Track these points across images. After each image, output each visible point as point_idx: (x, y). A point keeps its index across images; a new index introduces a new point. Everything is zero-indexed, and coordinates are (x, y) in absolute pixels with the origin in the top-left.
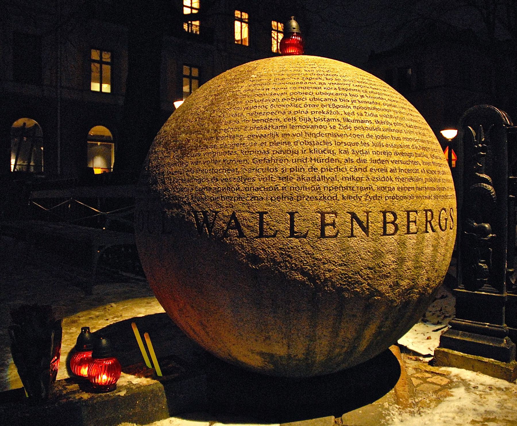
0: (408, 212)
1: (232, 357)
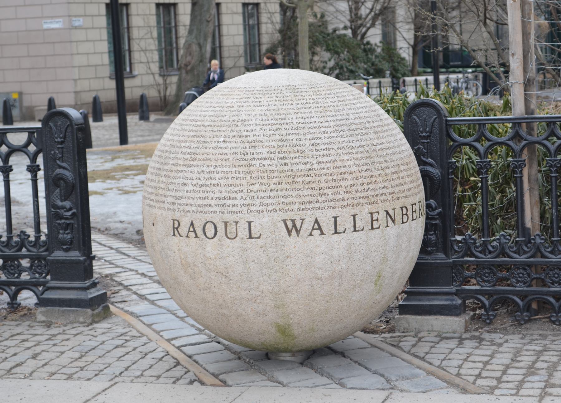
0: (372, 214)
1: (259, 350)
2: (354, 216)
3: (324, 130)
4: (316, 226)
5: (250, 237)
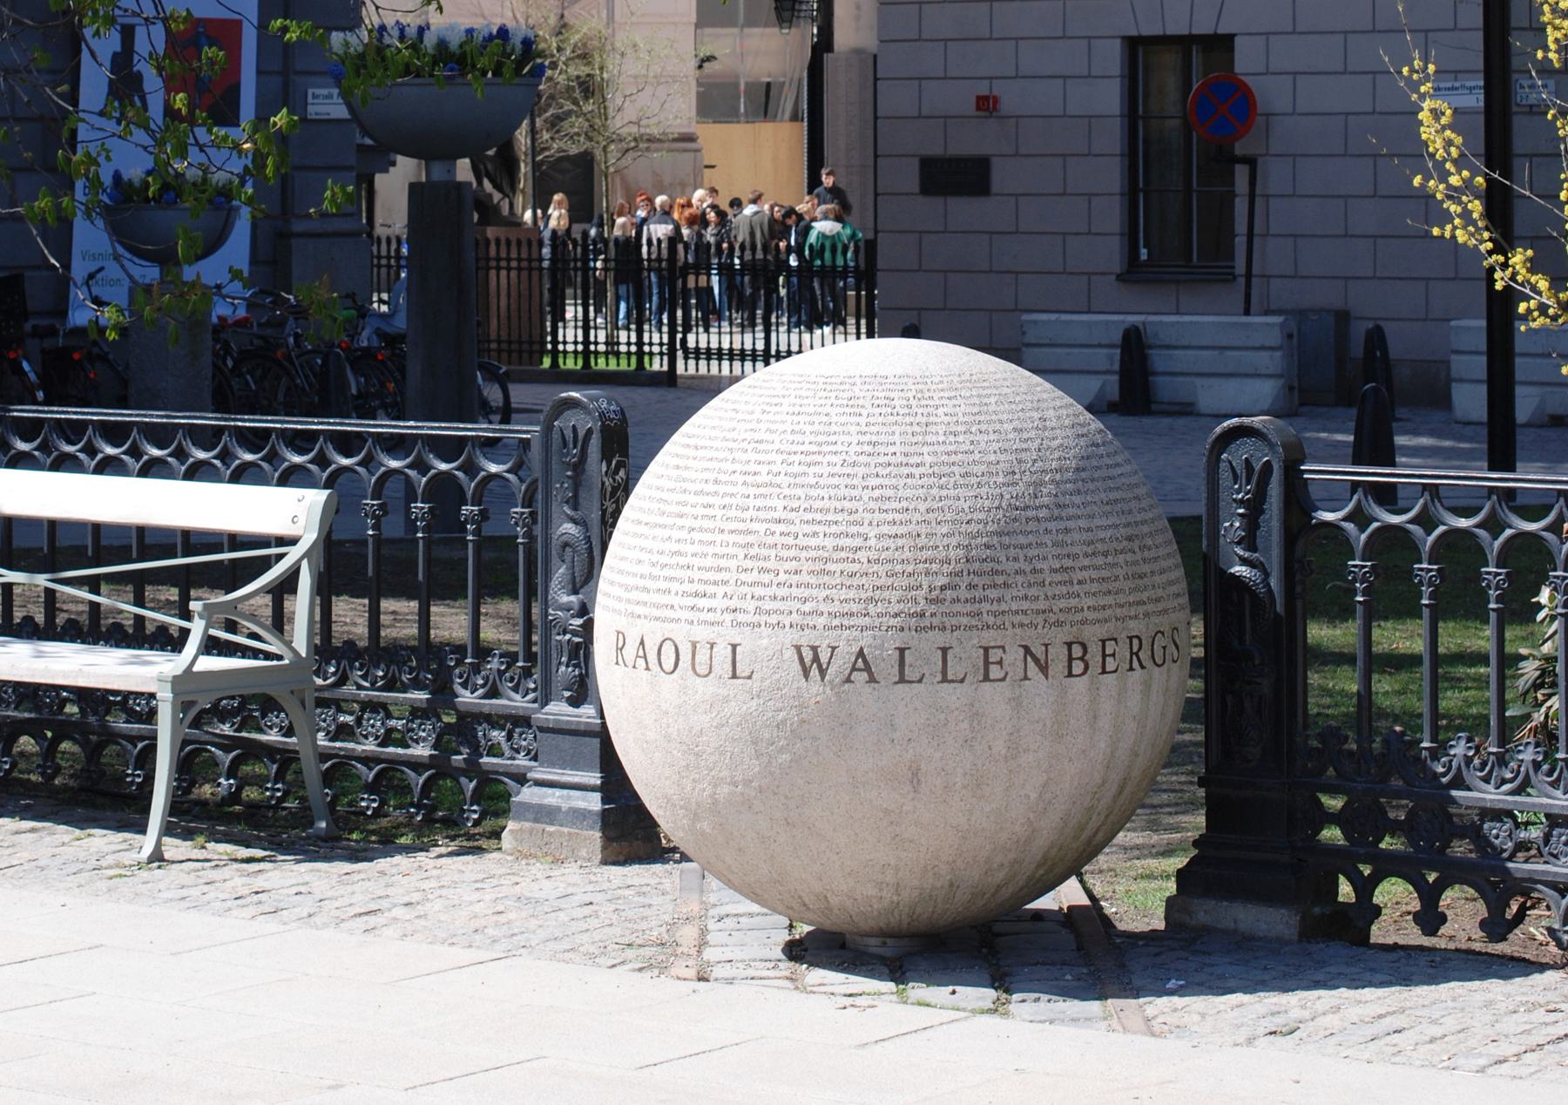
0: (986, 650)
2: (944, 651)
3: (906, 471)
4: (860, 663)
5: (734, 676)
